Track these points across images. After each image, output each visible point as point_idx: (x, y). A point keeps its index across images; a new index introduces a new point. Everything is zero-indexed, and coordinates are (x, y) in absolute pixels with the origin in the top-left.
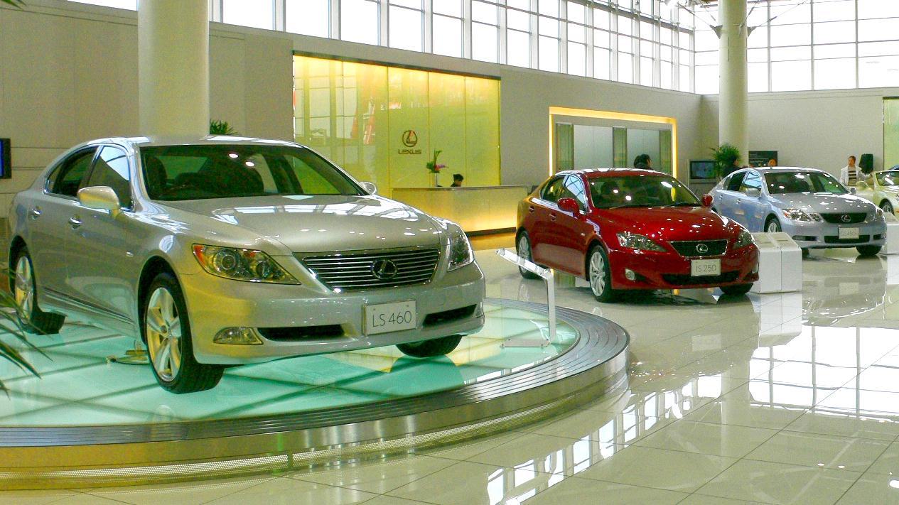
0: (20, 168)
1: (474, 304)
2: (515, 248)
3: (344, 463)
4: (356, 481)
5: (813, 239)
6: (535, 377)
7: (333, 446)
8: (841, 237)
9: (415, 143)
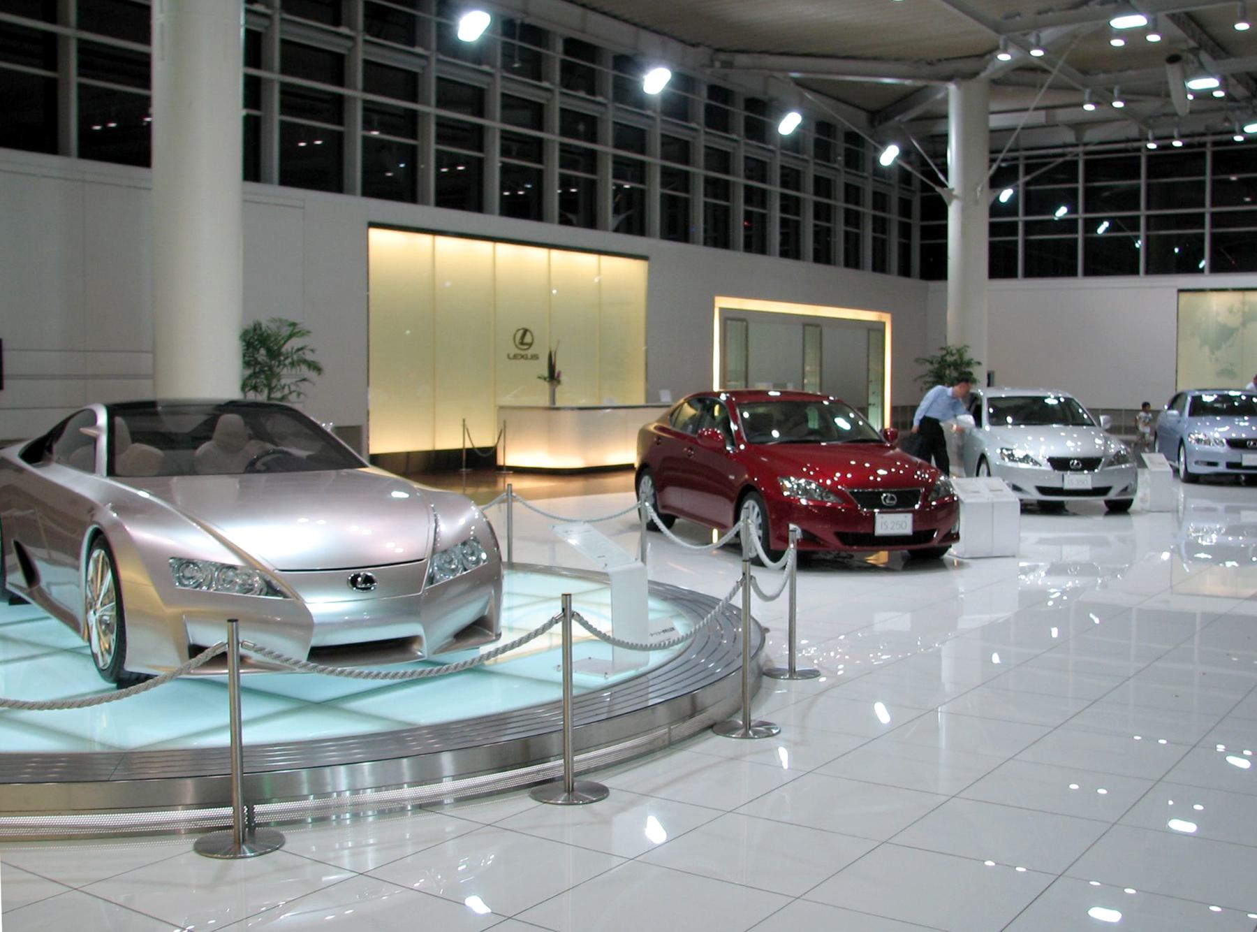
0: (15, 377)
1: (720, 552)
2: (634, 494)
3: (356, 816)
4: (371, 841)
5: (1214, 464)
6: (684, 676)
7: (339, 794)
8: (1244, 463)
9: (530, 345)
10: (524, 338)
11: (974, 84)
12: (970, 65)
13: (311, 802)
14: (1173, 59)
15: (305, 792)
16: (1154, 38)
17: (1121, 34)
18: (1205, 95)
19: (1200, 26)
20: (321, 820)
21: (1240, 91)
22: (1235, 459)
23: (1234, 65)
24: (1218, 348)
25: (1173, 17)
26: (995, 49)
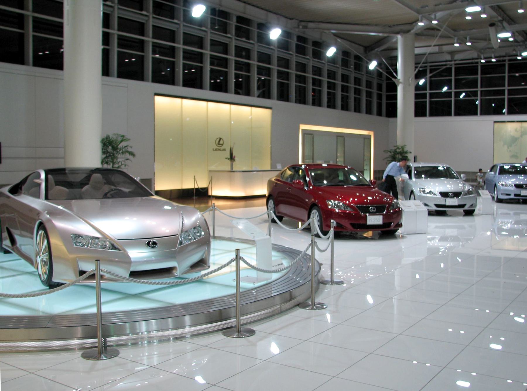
0: (6, 158)
1: (302, 232)
2: (266, 207)
3: (149, 342)
4: (156, 353)
5: (509, 195)
6: (287, 283)
7: (142, 333)
8: (522, 194)
9: (222, 145)
10: (220, 142)
11: (408, 35)
12: (407, 27)
13: (131, 336)
14: (492, 25)
15: (128, 332)
16: (484, 16)
17: (470, 14)
18: (505, 40)
19: (503, 11)
20: (135, 344)
21: (520, 38)
22: (518, 193)
23: (517, 27)
24: (511, 146)
25: (492, 7)
26: (417, 21)
